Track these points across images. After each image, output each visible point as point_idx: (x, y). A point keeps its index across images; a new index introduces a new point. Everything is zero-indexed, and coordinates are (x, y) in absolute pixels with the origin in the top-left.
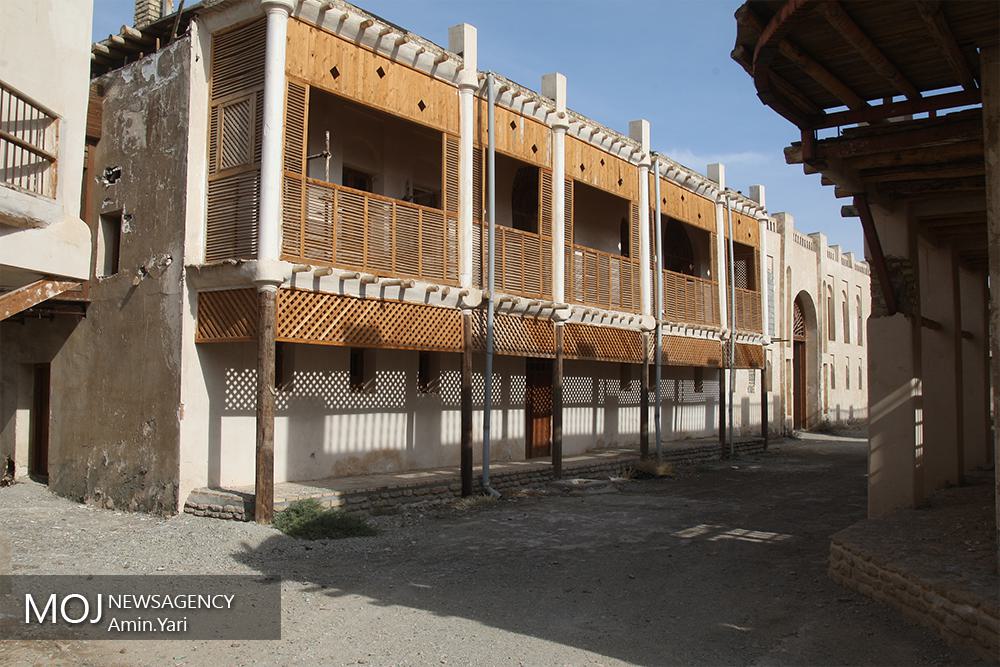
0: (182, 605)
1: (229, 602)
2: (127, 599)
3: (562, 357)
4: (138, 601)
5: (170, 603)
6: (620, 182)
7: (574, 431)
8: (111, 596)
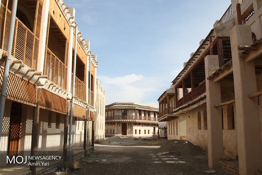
0: (48, 159)
1: (60, 158)
2: (33, 157)
3: (39, 107)
4: (36, 158)
5: (45, 158)
6: (65, 28)
7: (53, 146)
8: (29, 156)
